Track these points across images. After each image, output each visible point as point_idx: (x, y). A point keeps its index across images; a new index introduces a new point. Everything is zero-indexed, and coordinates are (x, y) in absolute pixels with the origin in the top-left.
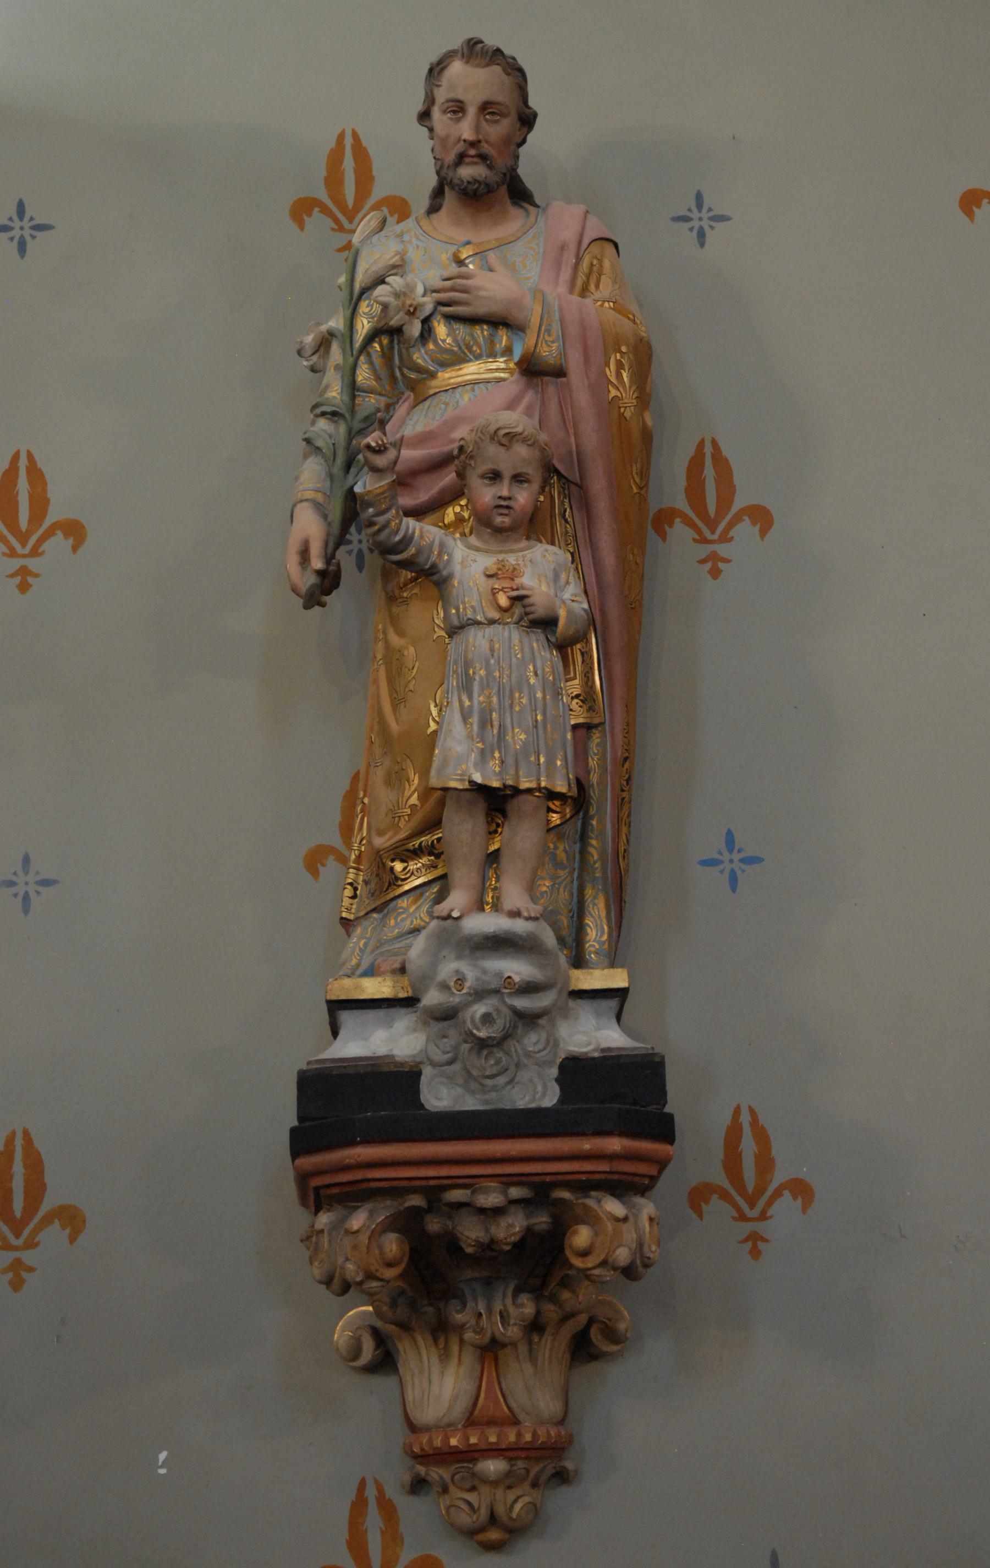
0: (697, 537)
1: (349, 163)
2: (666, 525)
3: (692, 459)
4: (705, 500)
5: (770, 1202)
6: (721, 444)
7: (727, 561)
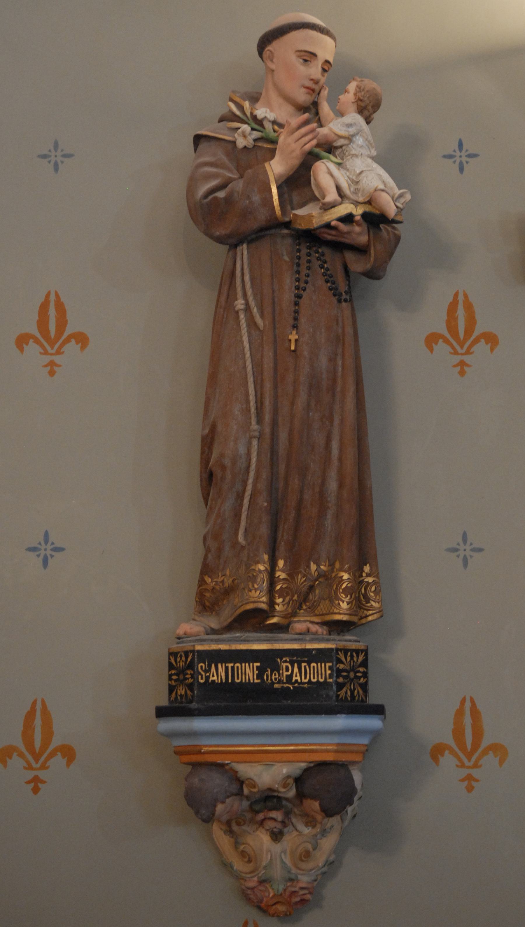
1: (52, 312)
2: (7, 758)
3: (28, 712)
4: (458, 328)
6: (61, 295)
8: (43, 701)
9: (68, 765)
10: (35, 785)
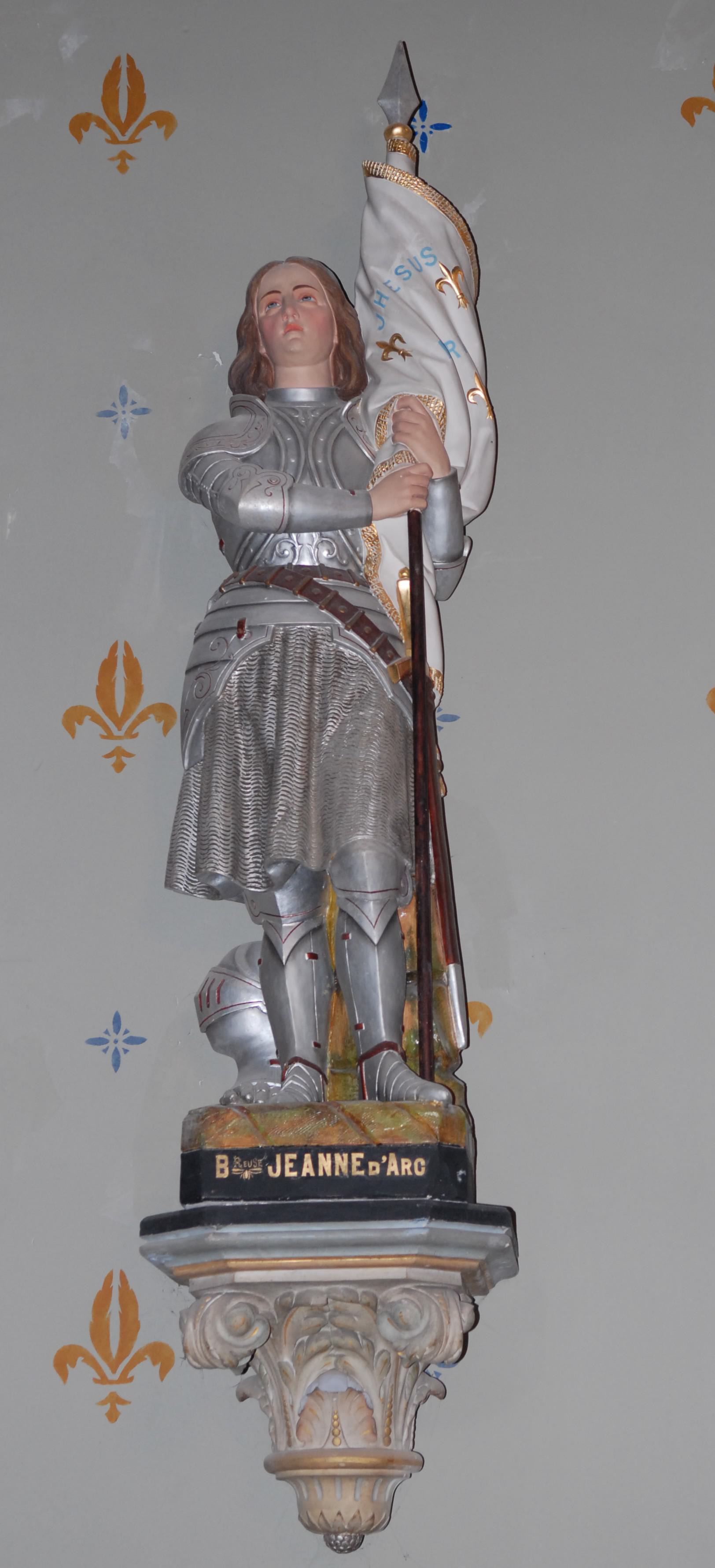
0: (98, 1377)
5: (135, 724)
6: (129, 1277)
7: (129, 755)
8: (123, 1276)
9: (163, 1373)
10: (111, 1408)
